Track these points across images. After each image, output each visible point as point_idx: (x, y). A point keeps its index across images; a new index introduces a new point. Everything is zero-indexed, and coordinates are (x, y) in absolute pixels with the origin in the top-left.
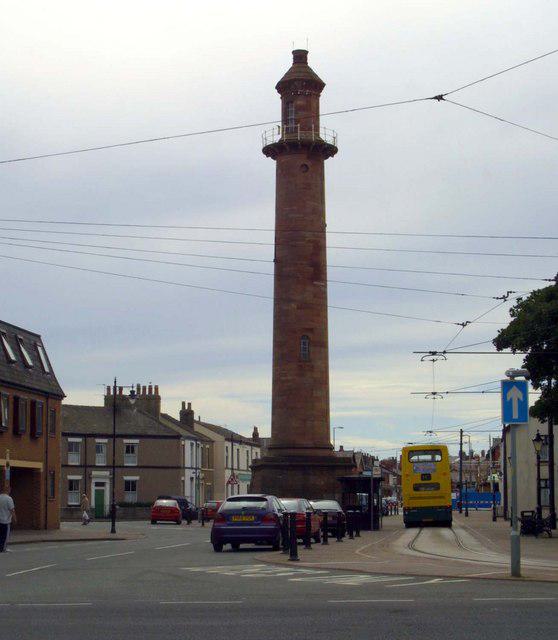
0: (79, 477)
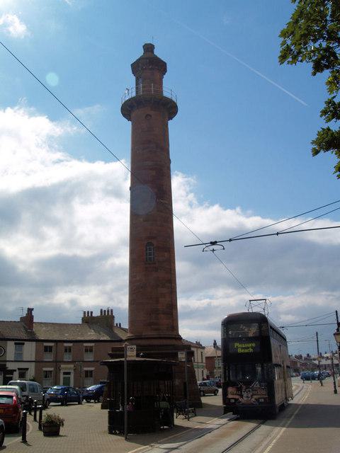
0: (52, 369)
